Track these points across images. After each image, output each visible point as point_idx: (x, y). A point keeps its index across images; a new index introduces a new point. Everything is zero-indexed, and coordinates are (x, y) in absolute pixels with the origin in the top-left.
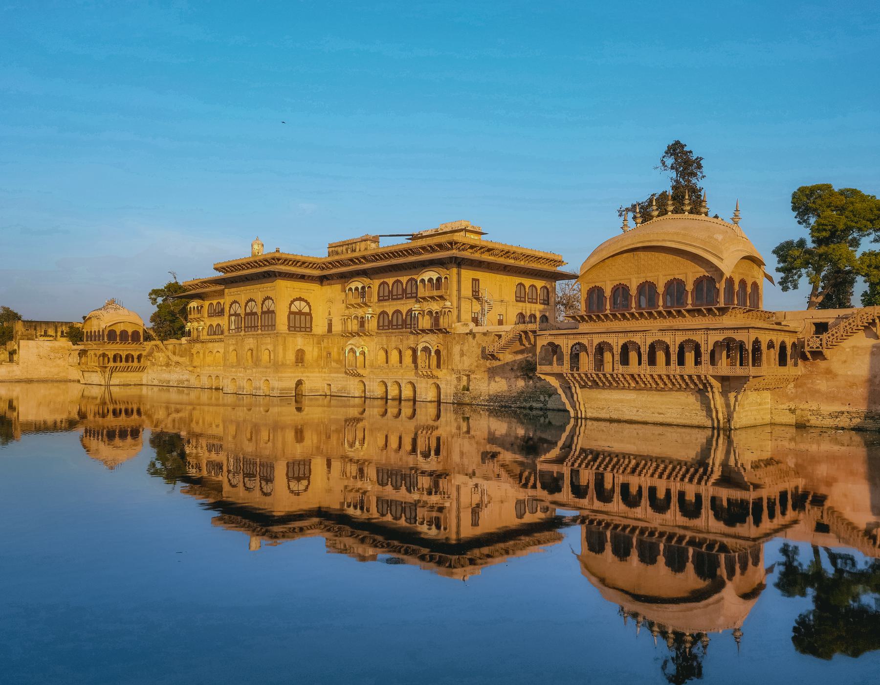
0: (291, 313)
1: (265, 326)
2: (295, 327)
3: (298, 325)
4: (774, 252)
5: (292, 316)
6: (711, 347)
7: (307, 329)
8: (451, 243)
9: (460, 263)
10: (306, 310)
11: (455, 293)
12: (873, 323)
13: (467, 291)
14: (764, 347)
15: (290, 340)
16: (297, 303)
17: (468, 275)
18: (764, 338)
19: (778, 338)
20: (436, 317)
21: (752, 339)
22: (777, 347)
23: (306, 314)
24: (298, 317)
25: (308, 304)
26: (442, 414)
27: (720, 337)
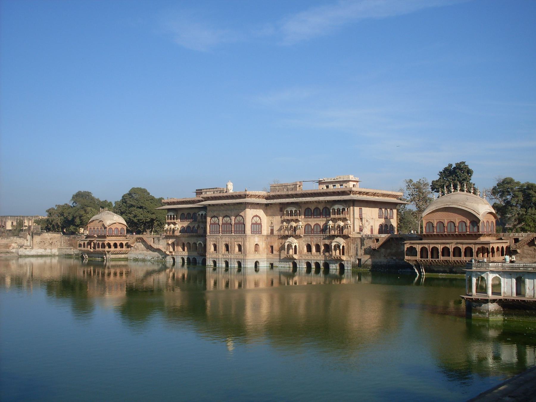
0: (252, 224)
1: (224, 231)
2: (254, 232)
3: (228, 230)
4: (47, 211)
5: (253, 226)
6: (476, 250)
7: (260, 232)
8: (350, 192)
9: (354, 203)
10: (259, 222)
11: (352, 216)
12: (533, 240)
13: (357, 215)
14: (495, 250)
15: (252, 238)
16: (255, 218)
17: (357, 209)
18: (495, 246)
19: (500, 246)
20: (342, 229)
21: (491, 247)
22: (500, 249)
23: (217, 224)
24: (255, 226)
25: (260, 218)
26: (151, 252)
27: (480, 246)
